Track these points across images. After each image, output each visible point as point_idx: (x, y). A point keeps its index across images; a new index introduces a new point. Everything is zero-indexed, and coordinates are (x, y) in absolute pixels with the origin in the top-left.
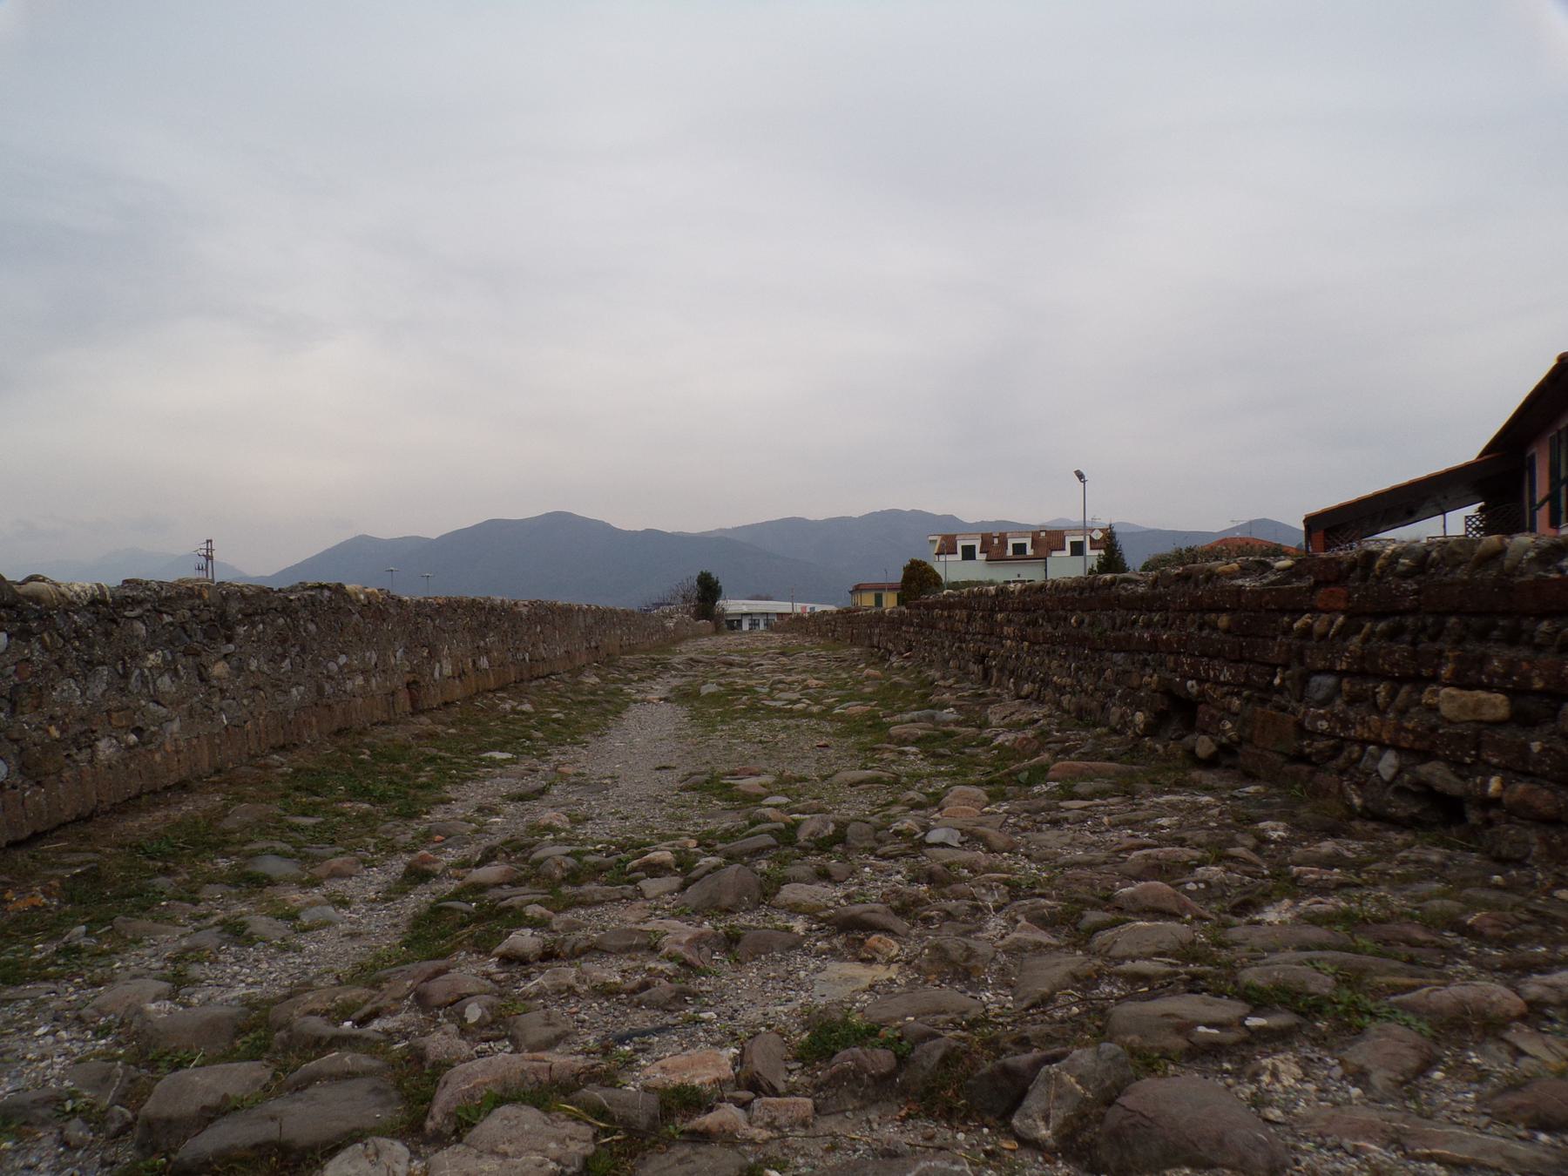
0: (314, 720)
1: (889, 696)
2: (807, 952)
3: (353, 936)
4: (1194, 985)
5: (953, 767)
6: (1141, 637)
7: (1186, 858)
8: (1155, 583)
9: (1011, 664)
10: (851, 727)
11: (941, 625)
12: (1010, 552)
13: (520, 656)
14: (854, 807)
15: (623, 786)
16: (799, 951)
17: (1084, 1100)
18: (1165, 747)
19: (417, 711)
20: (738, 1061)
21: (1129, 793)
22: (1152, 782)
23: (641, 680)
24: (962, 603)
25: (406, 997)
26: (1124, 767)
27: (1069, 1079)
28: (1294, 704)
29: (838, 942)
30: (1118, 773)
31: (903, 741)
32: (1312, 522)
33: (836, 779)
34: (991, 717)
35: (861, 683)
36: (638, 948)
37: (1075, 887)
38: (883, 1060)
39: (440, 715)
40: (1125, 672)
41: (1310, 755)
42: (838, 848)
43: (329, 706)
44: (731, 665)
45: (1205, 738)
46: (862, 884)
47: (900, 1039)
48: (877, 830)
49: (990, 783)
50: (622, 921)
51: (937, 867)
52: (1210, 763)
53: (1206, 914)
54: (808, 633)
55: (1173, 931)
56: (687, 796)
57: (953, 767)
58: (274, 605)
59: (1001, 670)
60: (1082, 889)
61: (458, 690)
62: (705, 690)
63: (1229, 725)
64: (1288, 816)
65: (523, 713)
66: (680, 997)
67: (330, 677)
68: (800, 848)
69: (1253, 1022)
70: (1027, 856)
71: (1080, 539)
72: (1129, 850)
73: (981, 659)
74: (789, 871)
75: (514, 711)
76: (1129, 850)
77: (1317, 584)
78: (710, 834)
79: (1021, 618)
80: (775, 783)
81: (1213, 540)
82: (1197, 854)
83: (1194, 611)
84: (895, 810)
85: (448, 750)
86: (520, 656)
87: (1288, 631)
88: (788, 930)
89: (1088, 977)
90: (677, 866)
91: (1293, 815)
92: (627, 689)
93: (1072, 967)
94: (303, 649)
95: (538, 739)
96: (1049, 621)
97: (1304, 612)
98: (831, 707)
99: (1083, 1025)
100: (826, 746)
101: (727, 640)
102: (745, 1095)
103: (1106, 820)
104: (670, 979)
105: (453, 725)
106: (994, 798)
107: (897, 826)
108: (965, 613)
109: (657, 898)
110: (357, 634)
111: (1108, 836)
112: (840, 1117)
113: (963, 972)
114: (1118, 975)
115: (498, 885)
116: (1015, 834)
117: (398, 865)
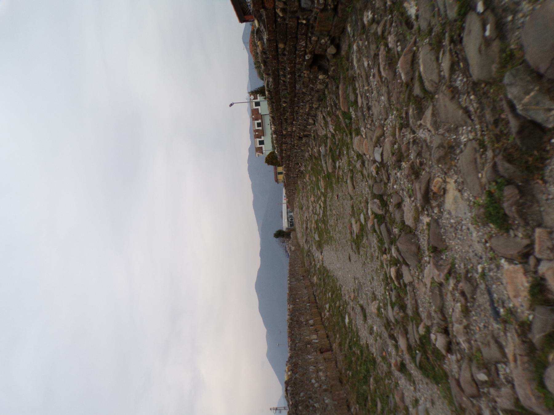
0: (337, 393)
1: (316, 171)
2: (440, 217)
3: (433, 403)
4: (457, 41)
5: (344, 148)
6: (290, 78)
7: (385, 53)
8: (268, 74)
9: (302, 127)
10: (329, 185)
11: (289, 153)
12: (260, 128)
13: (308, 308)
14: (364, 188)
15: (358, 276)
16: (440, 221)
17: (540, 91)
18: (332, 66)
19: (331, 349)
20: (510, 260)
21: (353, 79)
22: (348, 70)
23: (314, 260)
24: (280, 146)
25: (472, 402)
26: (342, 81)
27: (527, 99)
28: (313, 14)
29: (434, 203)
30: (344, 84)
31: (334, 167)
32: (242, 20)
33: (352, 194)
34: (323, 134)
35: (312, 181)
36: (441, 291)
37: (401, 100)
38: (510, 192)
39: (332, 339)
40: (303, 84)
41: (334, 5)
42: (385, 198)
43: (332, 386)
44: (307, 228)
45: (328, 50)
46: (403, 190)
47: (497, 183)
48: (376, 182)
49: (351, 134)
50: (425, 294)
51: (394, 158)
52: (338, 47)
53: (412, 41)
54: (294, 199)
55: (424, 55)
56: (362, 252)
57: (344, 148)
58: (294, 411)
59: (304, 131)
60: (402, 96)
61: (322, 332)
62: (317, 238)
63: (323, 41)
64: (361, 12)
65: (329, 308)
66: (469, 280)
67: (320, 386)
68: (386, 214)
69: (480, 8)
70: (386, 119)
71: (254, 103)
72: (381, 77)
73: (300, 138)
74: (398, 219)
75: (329, 311)
76: (381, 77)
77: (264, 7)
78: (380, 248)
79: (285, 124)
80: (355, 217)
81: (251, 57)
82: (382, 48)
83: (278, 59)
84: (365, 172)
85: (346, 339)
86: (308, 308)
87: (283, 19)
88: (428, 225)
89: (452, 92)
90: (397, 266)
91: (360, 10)
92: (318, 266)
93: (447, 100)
94: (310, 398)
95: (340, 304)
96: (285, 114)
97: (276, 13)
98: (321, 193)
99: (484, 93)
100: (338, 196)
101: (297, 226)
102: (532, 261)
103: (366, 88)
104: (458, 282)
105: (335, 335)
106: (358, 133)
107: (374, 174)
108: (284, 145)
109: (412, 276)
110: (303, 375)
111: (374, 87)
112: (544, 213)
113: (450, 151)
114: (450, 77)
115: (408, 339)
116: (374, 125)
117: (397, 373)
